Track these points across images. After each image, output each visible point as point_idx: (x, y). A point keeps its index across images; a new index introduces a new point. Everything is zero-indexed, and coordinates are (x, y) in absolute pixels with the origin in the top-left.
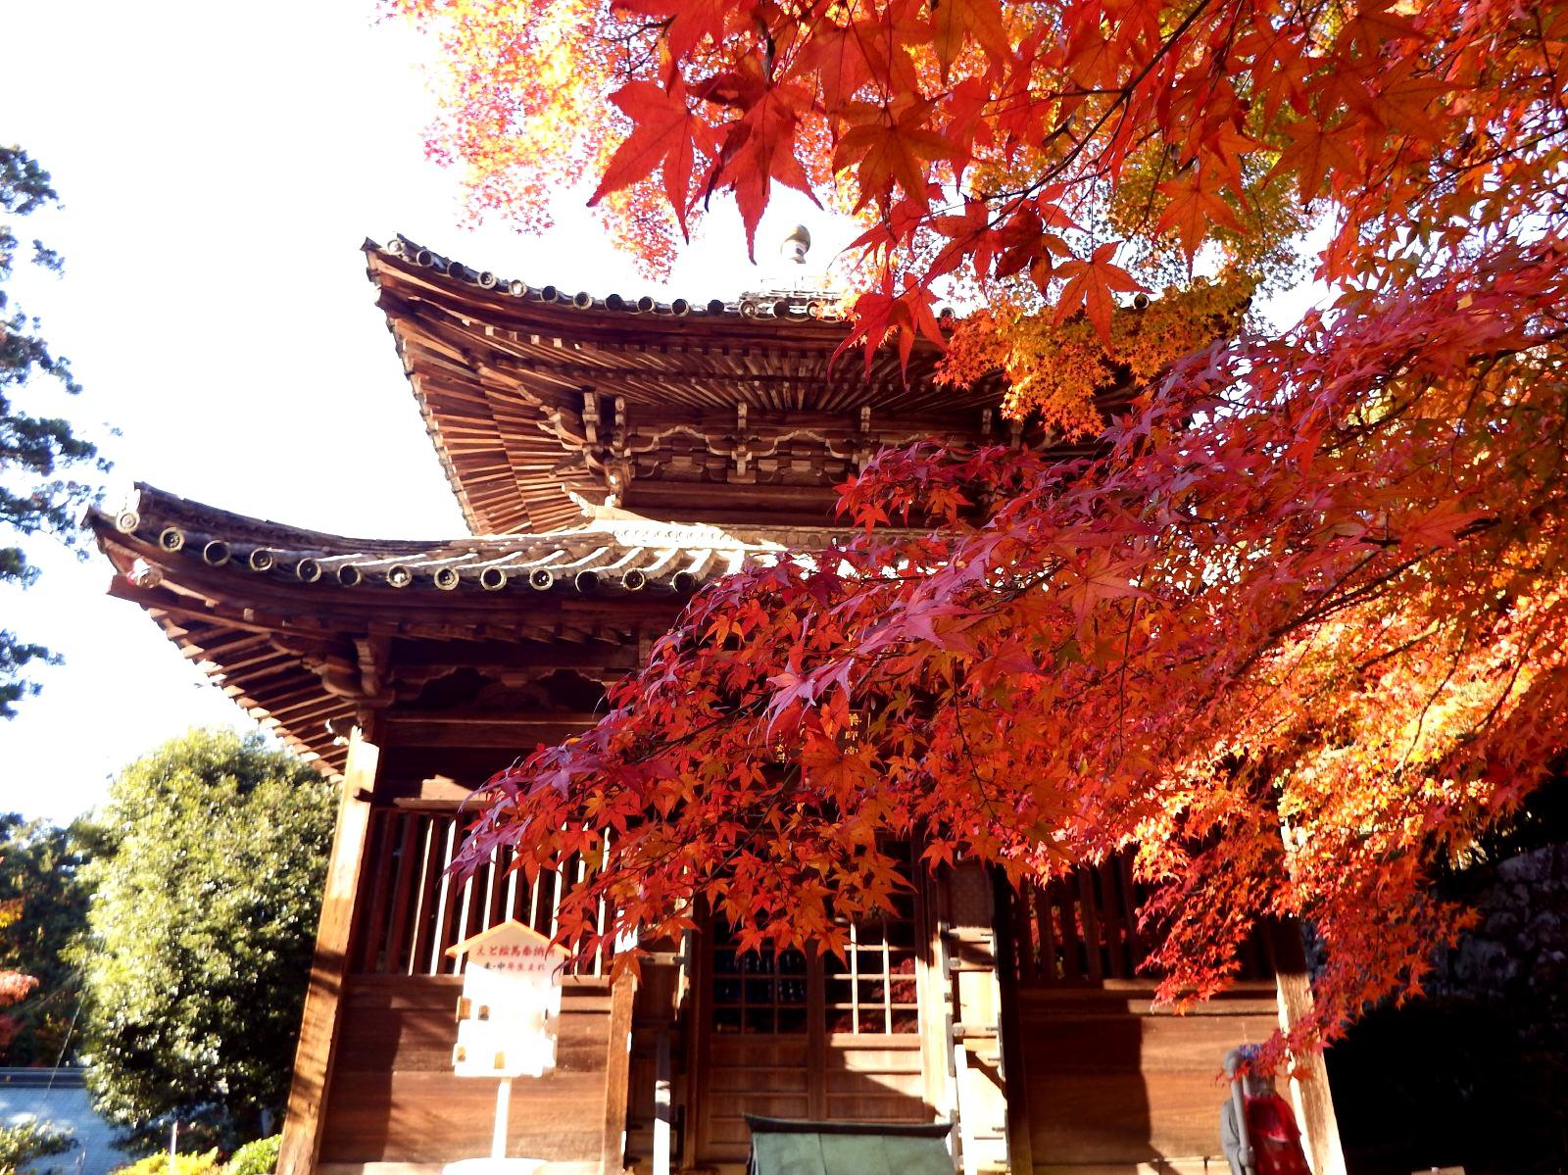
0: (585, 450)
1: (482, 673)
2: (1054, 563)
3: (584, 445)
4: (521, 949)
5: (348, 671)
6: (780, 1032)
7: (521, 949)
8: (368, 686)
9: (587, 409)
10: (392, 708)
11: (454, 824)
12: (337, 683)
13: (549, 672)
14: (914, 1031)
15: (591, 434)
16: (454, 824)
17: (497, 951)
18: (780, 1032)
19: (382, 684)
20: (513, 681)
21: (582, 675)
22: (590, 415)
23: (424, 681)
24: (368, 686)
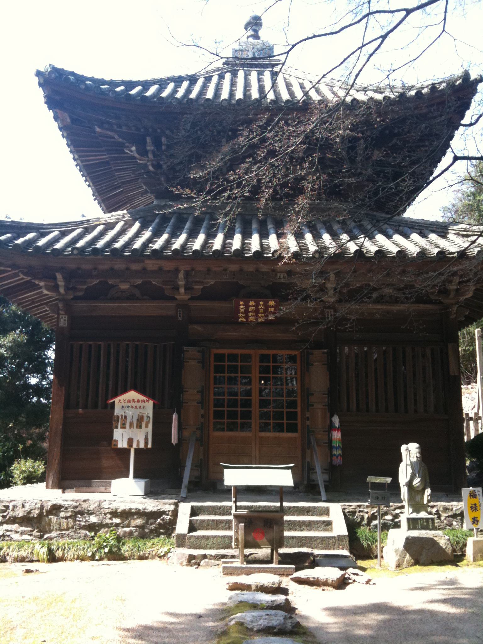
0: (148, 163)
1: (110, 283)
2: (310, 222)
3: (148, 161)
4: (136, 400)
5: (53, 284)
6: (251, 407)
7: (136, 400)
8: (62, 290)
9: (148, 144)
10: (73, 299)
11: (293, 465)
12: (47, 289)
13: (139, 282)
14: (137, 427)
15: (151, 156)
16: (293, 465)
17: (126, 401)
18: (251, 407)
19: (67, 289)
20: (124, 286)
21: (154, 283)
22: (150, 147)
23: (86, 287)
24: (62, 290)
